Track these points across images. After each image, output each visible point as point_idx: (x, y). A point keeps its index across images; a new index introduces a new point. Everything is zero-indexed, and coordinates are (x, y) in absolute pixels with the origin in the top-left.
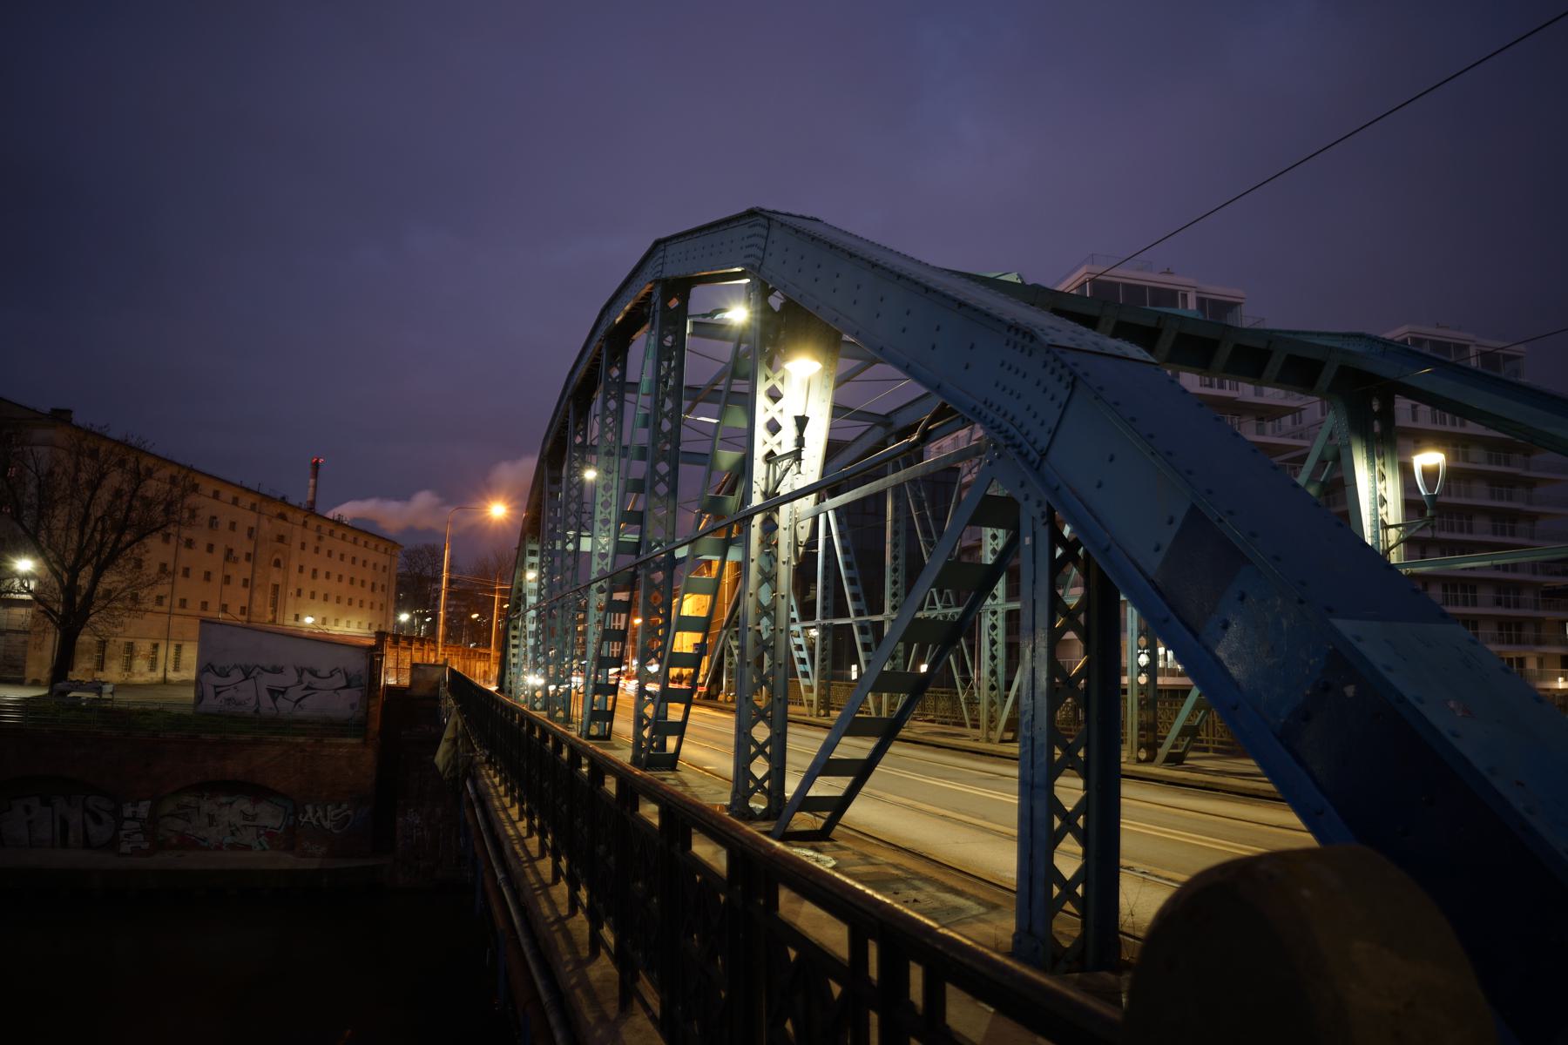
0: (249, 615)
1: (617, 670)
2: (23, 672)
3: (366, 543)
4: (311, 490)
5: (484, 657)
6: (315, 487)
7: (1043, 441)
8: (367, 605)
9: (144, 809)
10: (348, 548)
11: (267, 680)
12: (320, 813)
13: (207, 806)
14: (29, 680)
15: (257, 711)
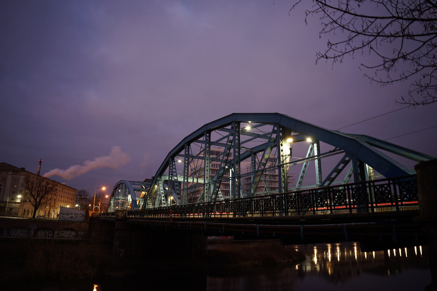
0: (50, 205)
1: (82, 201)
2: (18, 215)
3: (71, 190)
4: (39, 168)
5: (91, 210)
6: (40, 167)
7: (279, 123)
8: (70, 203)
9: (57, 232)
10: (67, 191)
11: (70, 216)
12: (81, 233)
13: (65, 232)
14: (19, 217)
15: (68, 220)
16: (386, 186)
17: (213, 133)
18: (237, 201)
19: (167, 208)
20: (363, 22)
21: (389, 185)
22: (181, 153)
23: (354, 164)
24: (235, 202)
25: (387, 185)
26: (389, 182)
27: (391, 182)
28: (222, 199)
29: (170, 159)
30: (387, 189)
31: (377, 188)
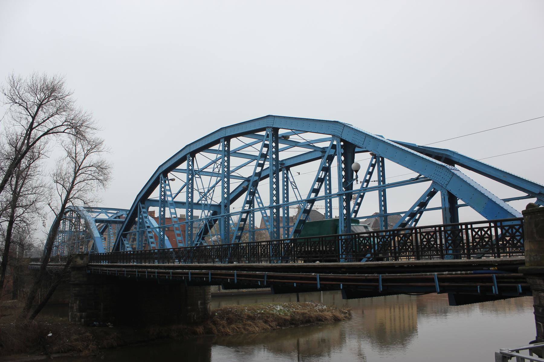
16: (486, 229)
17: (233, 141)
18: (285, 241)
19: (107, 254)
20: (61, 196)
21: (490, 228)
22: (179, 167)
23: (442, 197)
24: (185, 250)
25: (478, 230)
26: (490, 225)
27: (492, 225)
28: (153, 247)
29: (161, 176)
30: (519, 231)
31: (475, 232)
